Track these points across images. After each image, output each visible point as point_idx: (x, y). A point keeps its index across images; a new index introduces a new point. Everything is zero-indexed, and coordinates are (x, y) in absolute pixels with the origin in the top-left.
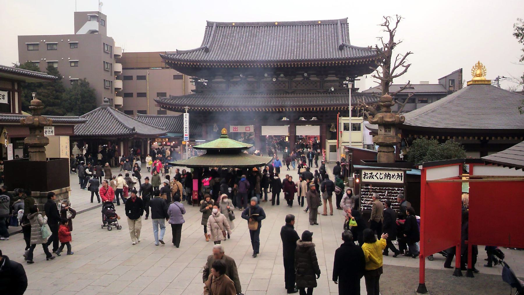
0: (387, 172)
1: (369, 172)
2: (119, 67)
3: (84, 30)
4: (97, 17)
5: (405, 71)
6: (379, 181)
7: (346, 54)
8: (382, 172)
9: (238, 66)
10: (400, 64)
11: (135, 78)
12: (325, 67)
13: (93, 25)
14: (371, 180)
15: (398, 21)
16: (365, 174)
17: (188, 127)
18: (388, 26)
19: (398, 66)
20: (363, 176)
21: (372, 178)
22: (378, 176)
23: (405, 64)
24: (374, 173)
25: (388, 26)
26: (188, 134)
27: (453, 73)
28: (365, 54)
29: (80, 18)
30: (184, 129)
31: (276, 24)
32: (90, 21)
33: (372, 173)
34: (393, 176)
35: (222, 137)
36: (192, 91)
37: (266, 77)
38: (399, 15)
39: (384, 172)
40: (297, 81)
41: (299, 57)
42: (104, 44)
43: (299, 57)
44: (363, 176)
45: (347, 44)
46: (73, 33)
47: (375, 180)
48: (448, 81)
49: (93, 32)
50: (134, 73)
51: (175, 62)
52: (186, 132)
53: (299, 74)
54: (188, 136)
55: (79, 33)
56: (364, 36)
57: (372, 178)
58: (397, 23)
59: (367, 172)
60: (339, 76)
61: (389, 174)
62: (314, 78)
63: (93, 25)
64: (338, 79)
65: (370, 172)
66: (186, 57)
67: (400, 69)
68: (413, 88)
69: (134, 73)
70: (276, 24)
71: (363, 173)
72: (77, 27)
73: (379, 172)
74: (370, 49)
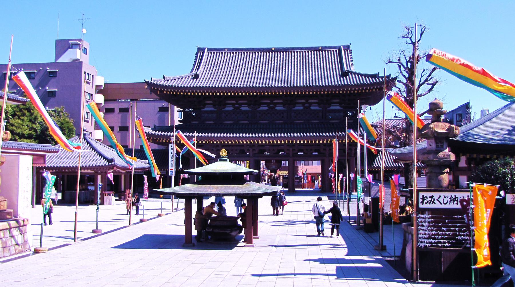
3: (66, 58)
5: (430, 90)
6: (443, 206)
10: (426, 80)
11: (117, 111)
12: (328, 95)
14: (432, 206)
15: (422, 33)
16: (423, 198)
18: (410, 38)
19: (423, 83)
20: (420, 200)
21: (434, 202)
22: (441, 200)
23: (431, 82)
25: (410, 38)
27: (460, 108)
29: (63, 46)
30: (170, 163)
31: (273, 49)
32: (72, 48)
33: (432, 197)
35: (220, 160)
36: (179, 121)
38: (423, 26)
40: (298, 110)
42: (85, 72)
44: (420, 200)
45: (352, 70)
46: (51, 59)
47: (437, 205)
48: (455, 115)
51: (161, 89)
52: (172, 166)
55: (60, 60)
56: (367, 63)
57: (434, 202)
58: (421, 35)
60: (343, 105)
61: (456, 197)
64: (342, 108)
66: (174, 84)
67: (425, 88)
71: (421, 197)
72: (57, 56)
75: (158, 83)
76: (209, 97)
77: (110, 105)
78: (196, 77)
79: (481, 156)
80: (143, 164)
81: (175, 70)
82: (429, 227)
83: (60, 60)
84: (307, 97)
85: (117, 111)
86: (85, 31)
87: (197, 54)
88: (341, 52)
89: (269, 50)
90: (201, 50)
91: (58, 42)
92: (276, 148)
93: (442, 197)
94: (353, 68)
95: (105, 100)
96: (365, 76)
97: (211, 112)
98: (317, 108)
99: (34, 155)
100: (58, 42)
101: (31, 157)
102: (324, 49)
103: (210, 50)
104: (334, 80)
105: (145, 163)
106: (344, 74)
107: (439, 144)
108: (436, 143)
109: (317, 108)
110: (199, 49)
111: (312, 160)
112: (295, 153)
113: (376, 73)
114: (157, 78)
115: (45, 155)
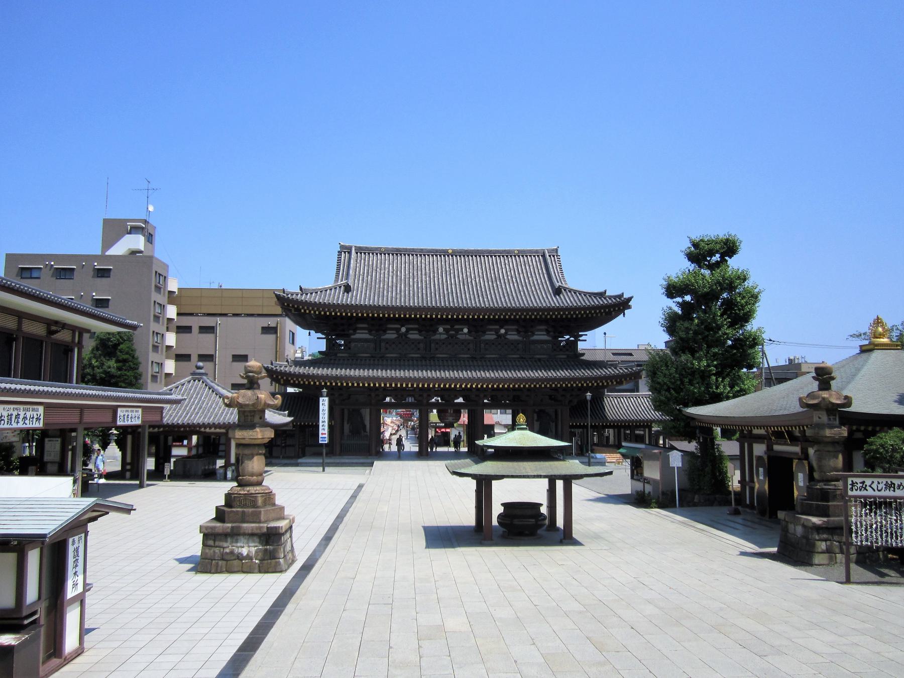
0: (889, 481)
1: (859, 480)
2: (172, 312)
3: (120, 249)
4: (143, 228)
6: (877, 493)
7: (566, 301)
8: (880, 480)
9: (587, 315)
11: (195, 330)
13: (137, 242)
14: (864, 493)
16: (853, 484)
17: (326, 420)
20: (850, 487)
21: (865, 489)
22: (874, 486)
24: (868, 481)
26: (326, 431)
28: (597, 302)
29: (114, 229)
31: (450, 251)
32: (130, 233)
33: (863, 483)
34: (899, 486)
37: (440, 334)
39: (884, 480)
41: (370, 300)
43: (370, 300)
44: (850, 487)
46: (99, 252)
49: (134, 253)
50: (194, 322)
53: (491, 330)
54: (326, 436)
55: (110, 252)
57: (865, 489)
59: (855, 480)
62: (414, 336)
63: (137, 242)
65: (861, 480)
68: (631, 354)
69: (194, 322)
70: (450, 251)
71: (850, 482)
72: (108, 243)
73: (876, 480)
74: (602, 295)
75: (294, 296)
76: (362, 319)
77: (186, 321)
78: (348, 289)
79: (870, 428)
80: (281, 417)
81: (313, 275)
82: (881, 515)
83: (110, 252)
84: (502, 322)
85: (195, 330)
86: (151, 208)
87: (340, 253)
88: (547, 258)
89: (444, 253)
90: (345, 250)
91: (107, 222)
92: (448, 393)
93: (876, 483)
94: (565, 281)
95: (178, 314)
96: (585, 294)
97: (366, 340)
98: (516, 337)
99: (143, 408)
100: (107, 222)
101: (140, 410)
102: (522, 253)
103: (359, 250)
104: (544, 299)
105: (284, 415)
106: (558, 291)
107: (831, 417)
108: (828, 415)
109: (516, 337)
110: (342, 247)
111: (497, 409)
112: (478, 399)
113: (601, 290)
114: (292, 288)
115: (163, 408)
